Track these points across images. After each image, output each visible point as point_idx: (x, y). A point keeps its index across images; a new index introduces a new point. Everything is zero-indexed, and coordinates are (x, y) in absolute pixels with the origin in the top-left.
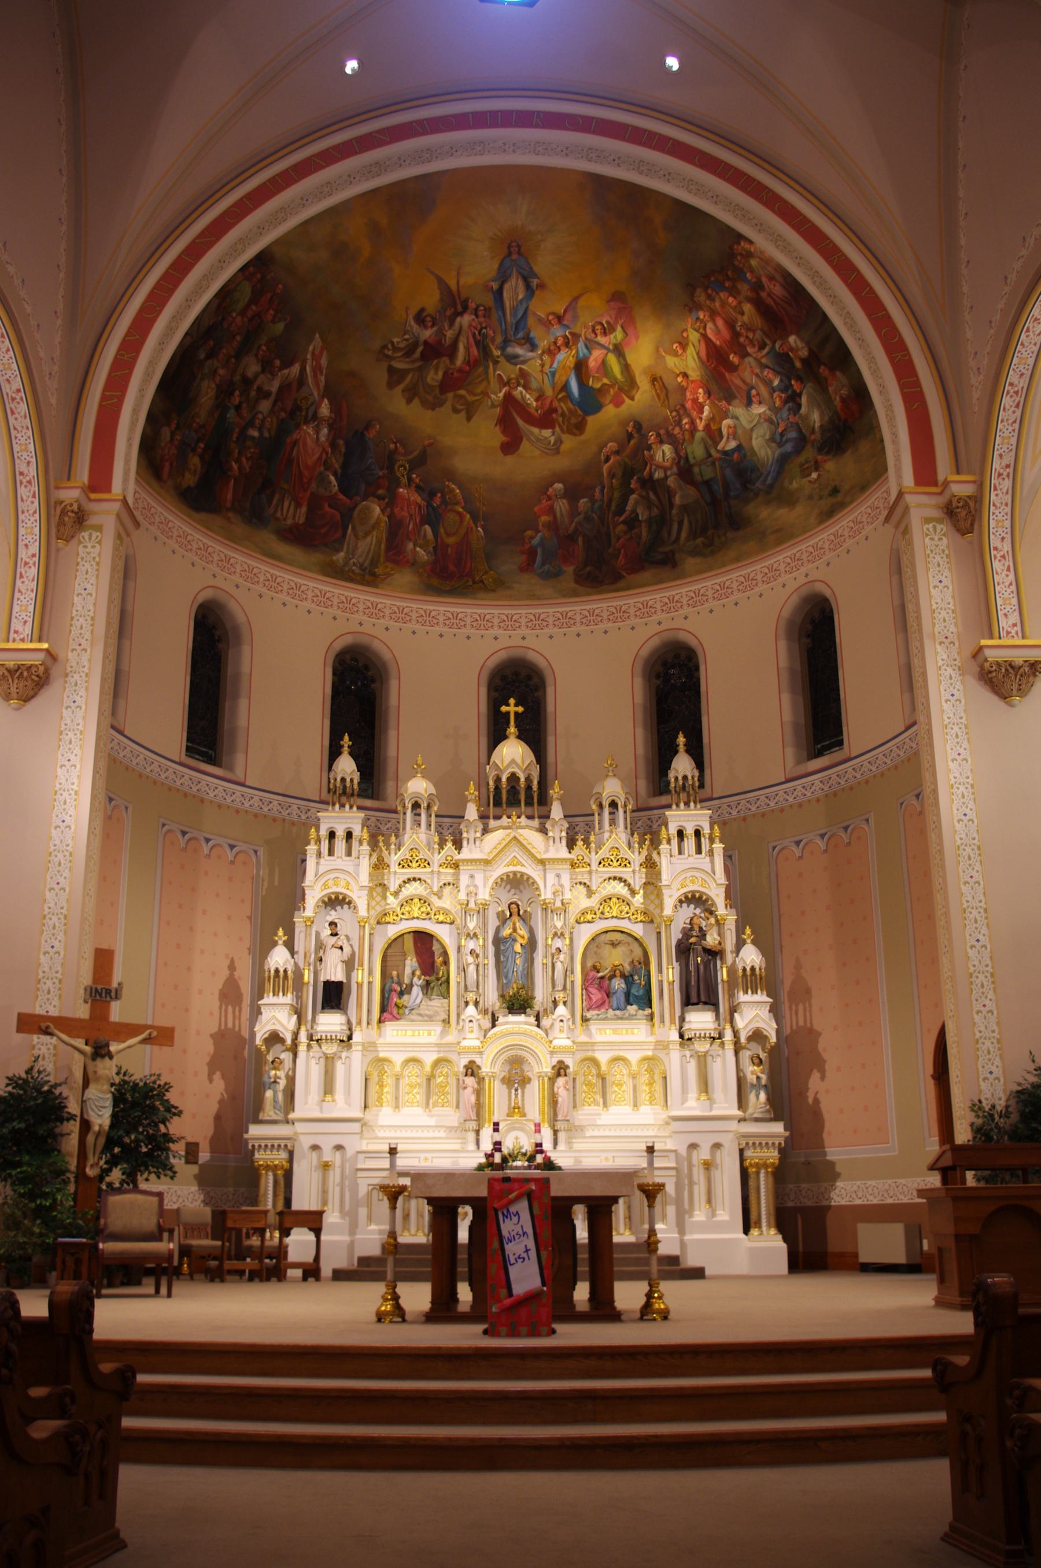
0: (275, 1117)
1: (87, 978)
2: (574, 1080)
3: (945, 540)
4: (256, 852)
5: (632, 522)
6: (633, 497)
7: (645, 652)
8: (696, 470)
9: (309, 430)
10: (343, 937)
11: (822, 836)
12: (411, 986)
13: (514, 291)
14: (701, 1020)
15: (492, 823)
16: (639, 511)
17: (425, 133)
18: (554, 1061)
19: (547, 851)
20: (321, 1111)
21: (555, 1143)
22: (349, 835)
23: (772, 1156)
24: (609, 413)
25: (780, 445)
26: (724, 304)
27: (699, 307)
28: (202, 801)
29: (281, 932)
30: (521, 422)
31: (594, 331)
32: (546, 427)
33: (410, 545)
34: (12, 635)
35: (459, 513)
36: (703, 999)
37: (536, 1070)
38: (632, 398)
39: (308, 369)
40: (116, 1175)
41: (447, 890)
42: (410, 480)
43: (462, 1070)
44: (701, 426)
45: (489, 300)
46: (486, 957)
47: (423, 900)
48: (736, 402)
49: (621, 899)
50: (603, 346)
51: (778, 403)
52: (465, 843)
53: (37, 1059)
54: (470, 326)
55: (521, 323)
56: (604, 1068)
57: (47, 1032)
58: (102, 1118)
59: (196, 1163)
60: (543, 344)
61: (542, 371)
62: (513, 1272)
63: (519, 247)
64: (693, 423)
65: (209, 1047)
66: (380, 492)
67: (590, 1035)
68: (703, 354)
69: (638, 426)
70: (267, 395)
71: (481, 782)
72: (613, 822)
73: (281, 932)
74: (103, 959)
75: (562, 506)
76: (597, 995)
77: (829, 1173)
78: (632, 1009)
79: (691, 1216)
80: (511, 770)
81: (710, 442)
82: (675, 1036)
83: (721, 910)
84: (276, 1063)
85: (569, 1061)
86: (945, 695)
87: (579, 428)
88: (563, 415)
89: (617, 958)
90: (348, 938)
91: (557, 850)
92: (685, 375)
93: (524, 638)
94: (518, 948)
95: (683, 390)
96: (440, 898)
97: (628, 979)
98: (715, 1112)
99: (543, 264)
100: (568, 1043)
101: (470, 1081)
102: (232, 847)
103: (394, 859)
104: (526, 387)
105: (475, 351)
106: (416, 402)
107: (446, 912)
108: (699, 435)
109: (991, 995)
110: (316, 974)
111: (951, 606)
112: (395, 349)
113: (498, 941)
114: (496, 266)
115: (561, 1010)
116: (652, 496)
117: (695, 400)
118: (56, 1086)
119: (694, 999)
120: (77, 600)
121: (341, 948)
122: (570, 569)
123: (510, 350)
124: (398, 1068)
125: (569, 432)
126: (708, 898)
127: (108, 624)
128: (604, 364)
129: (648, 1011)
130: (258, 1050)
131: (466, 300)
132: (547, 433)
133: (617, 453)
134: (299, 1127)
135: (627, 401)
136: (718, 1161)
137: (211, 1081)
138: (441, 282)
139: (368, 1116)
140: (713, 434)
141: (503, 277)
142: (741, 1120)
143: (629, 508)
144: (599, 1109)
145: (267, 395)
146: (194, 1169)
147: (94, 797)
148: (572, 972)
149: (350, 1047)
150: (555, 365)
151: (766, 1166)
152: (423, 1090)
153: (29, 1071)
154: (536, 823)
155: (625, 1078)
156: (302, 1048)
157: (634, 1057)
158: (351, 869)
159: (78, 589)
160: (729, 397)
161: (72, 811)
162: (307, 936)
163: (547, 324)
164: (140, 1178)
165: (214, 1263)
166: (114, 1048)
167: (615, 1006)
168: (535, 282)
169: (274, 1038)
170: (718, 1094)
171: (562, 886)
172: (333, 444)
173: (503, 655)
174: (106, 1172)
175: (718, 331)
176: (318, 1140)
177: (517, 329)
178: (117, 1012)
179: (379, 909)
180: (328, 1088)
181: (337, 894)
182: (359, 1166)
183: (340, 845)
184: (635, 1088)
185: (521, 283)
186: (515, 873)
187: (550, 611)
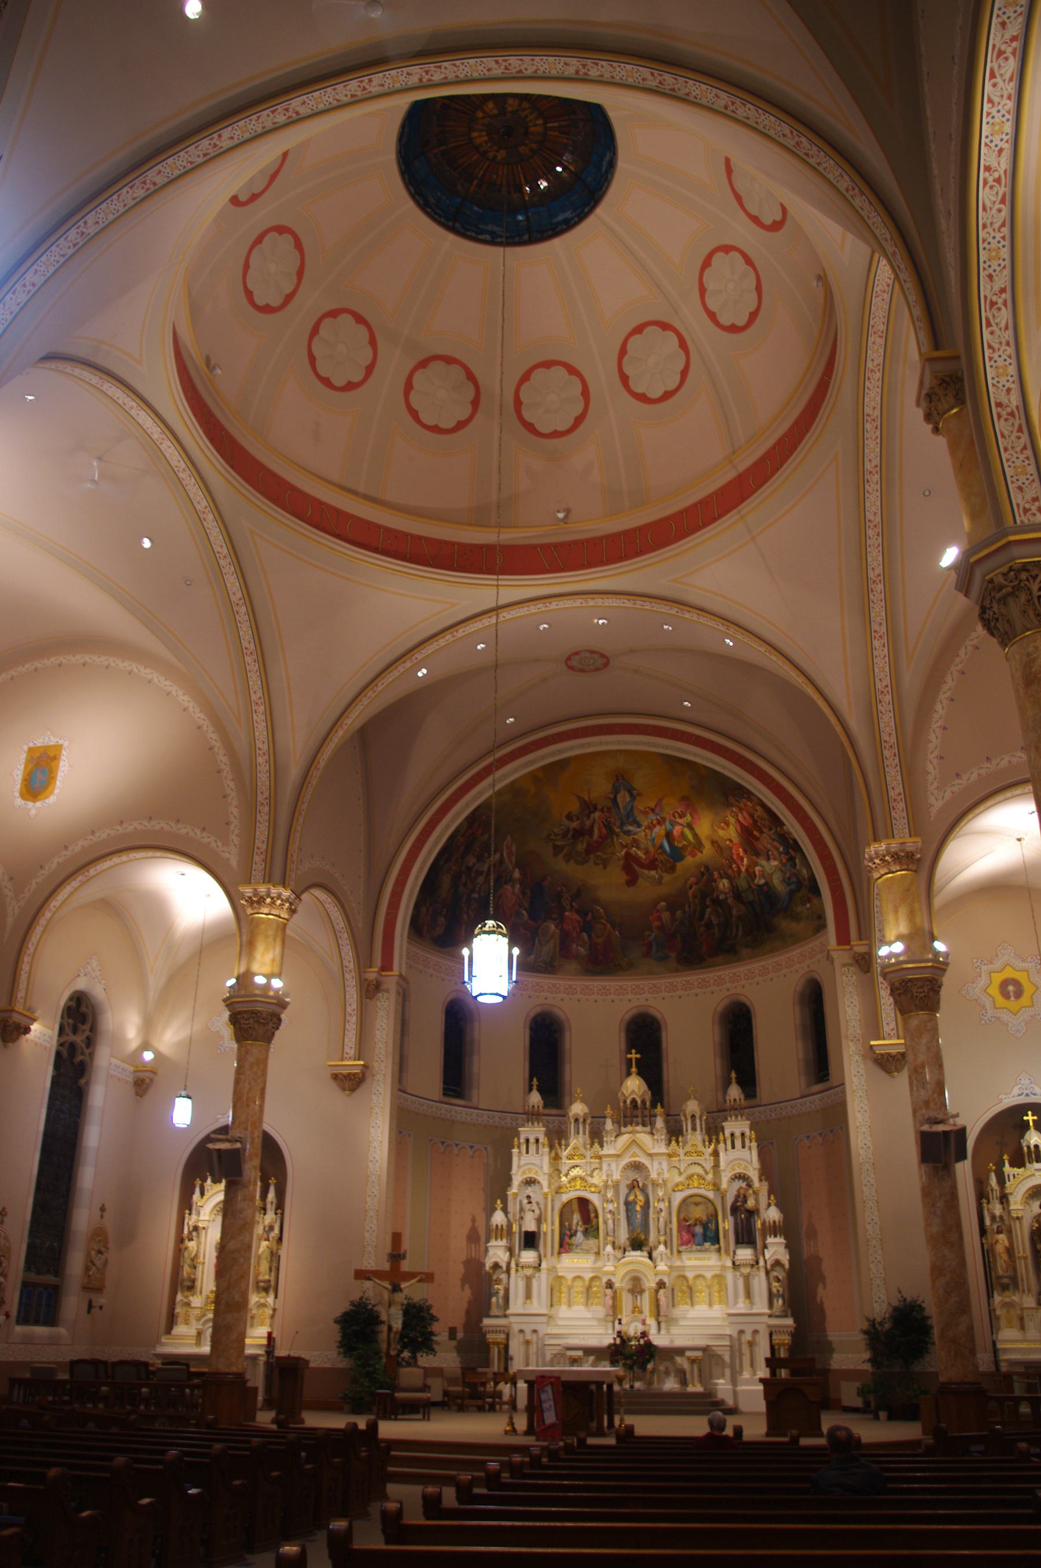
0: (497, 1314)
1: (388, 1249)
2: (673, 1290)
3: (855, 977)
4: (486, 1148)
5: (709, 925)
6: (708, 910)
7: (720, 1009)
8: (743, 895)
9: (508, 887)
10: (534, 1204)
11: (820, 1134)
12: (576, 1231)
13: (623, 798)
14: (745, 1254)
15: (623, 1129)
16: (713, 918)
17: (555, 743)
18: (657, 1279)
19: (653, 1148)
20: (524, 1309)
21: (659, 1329)
22: (537, 1141)
23: (787, 1339)
24: (689, 860)
25: (789, 885)
26: (745, 805)
27: (732, 805)
28: (453, 1122)
29: (499, 1202)
30: (636, 868)
31: (674, 816)
32: (652, 869)
33: (574, 946)
34: (345, 1055)
35: (603, 924)
36: (746, 1240)
37: (647, 1285)
38: (702, 853)
39: (505, 854)
40: (406, 1354)
41: (597, 1171)
42: (572, 906)
43: (604, 1284)
44: (743, 869)
45: (609, 804)
46: (619, 1214)
47: (582, 1179)
48: (762, 857)
49: (700, 1176)
50: (681, 824)
51: (784, 861)
52: (605, 1144)
53: (365, 1292)
54: (600, 818)
55: (630, 813)
56: (690, 1282)
57: (369, 1279)
58: (398, 1324)
59: (455, 1339)
60: (645, 823)
61: (646, 839)
62: (546, 1415)
63: (622, 776)
64: (738, 867)
65: (460, 1269)
66: (554, 916)
67: (682, 1261)
68: (739, 830)
69: (707, 868)
70: (481, 873)
71: (615, 1107)
72: (694, 1129)
73: (499, 1202)
74: (397, 1238)
75: (666, 916)
76: (686, 1236)
77: (827, 1348)
78: (707, 1245)
79: (741, 1375)
80: (632, 1097)
81: (749, 879)
82: (729, 1264)
83: (756, 1184)
84: (499, 1281)
85: (666, 1280)
86: (854, 1072)
87: (672, 869)
88: (662, 862)
89: (698, 1213)
90: (538, 1203)
91: (659, 1147)
92: (730, 840)
93: (647, 1000)
94: (638, 1208)
95: (731, 849)
96: (592, 1177)
97: (705, 1226)
98: (754, 1311)
99: (638, 783)
100: (665, 1268)
101: (609, 1291)
102: (471, 1147)
103: (565, 1154)
104: (637, 847)
105: (604, 831)
106: (572, 862)
107: (596, 1186)
108: (743, 875)
109: (880, 1252)
110: (520, 1226)
111: (858, 1018)
112: (556, 835)
113: (627, 1203)
114: (610, 786)
115: (662, 1248)
116: (720, 910)
117: (738, 855)
118: (374, 1306)
119: (741, 1241)
120: (378, 1033)
121: (533, 1211)
122: (673, 955)
123: (625, 828)
124: (569, 1283)
125: (666, 871)
126: (749, 1177)
127: (394, 1045)
128: (682, 834)
129: (717, 1246)
130: (489, 1273)
131: (596, 805)
132: (653, 873)
133: (696, 883)
134: (512, 1319)
135: (699, 854)
136: (757, 1341)
137: (463, 1289)
138: (579, 798)
139: (553, 1312)
140: (752, 875)
141: (616, 791)
142: (770, 1316)
143: (706, 917)
144: (687, 1307)
145: (481, 873)
146: (454, 1343)
147: (390, 1142)
148: (671, 1222)
149: (539, 1270)
150: (654, 835)
151: (783, 1345)
152: (585, 1295)
153: (361, 1299)
154: (648, 1129)
155: (704, 1288)
156: (513, 1272)
157: (709, 1275)
158: (538, 1162)
159: (378, 1026)
160: (757, 854)
161: (378, 1152)
162: (515, 1203)
163: (645, 813)
164: (418, 1355)
165: (459, 1401)
166: (403, 1285)
167: (696, 1243)
168: (635, 792)
169: (496, 1266)
170: (757, 1299)
171: (662, 1169)
172: (523, 893)
173: (634, 1012)
174: (401, 1351)
175: (745, 819)
176: (523, 1327)
177: (628, 816)
178: (405, 1266)
179: (557, 1184)
180: (528, 1296)
181: (531, 1178)
182: (546, 1343)
183: (532, 1147)
184: (710, 1295)
185: (627, 794)
186: (635, 1162)
187: (663, 982)
